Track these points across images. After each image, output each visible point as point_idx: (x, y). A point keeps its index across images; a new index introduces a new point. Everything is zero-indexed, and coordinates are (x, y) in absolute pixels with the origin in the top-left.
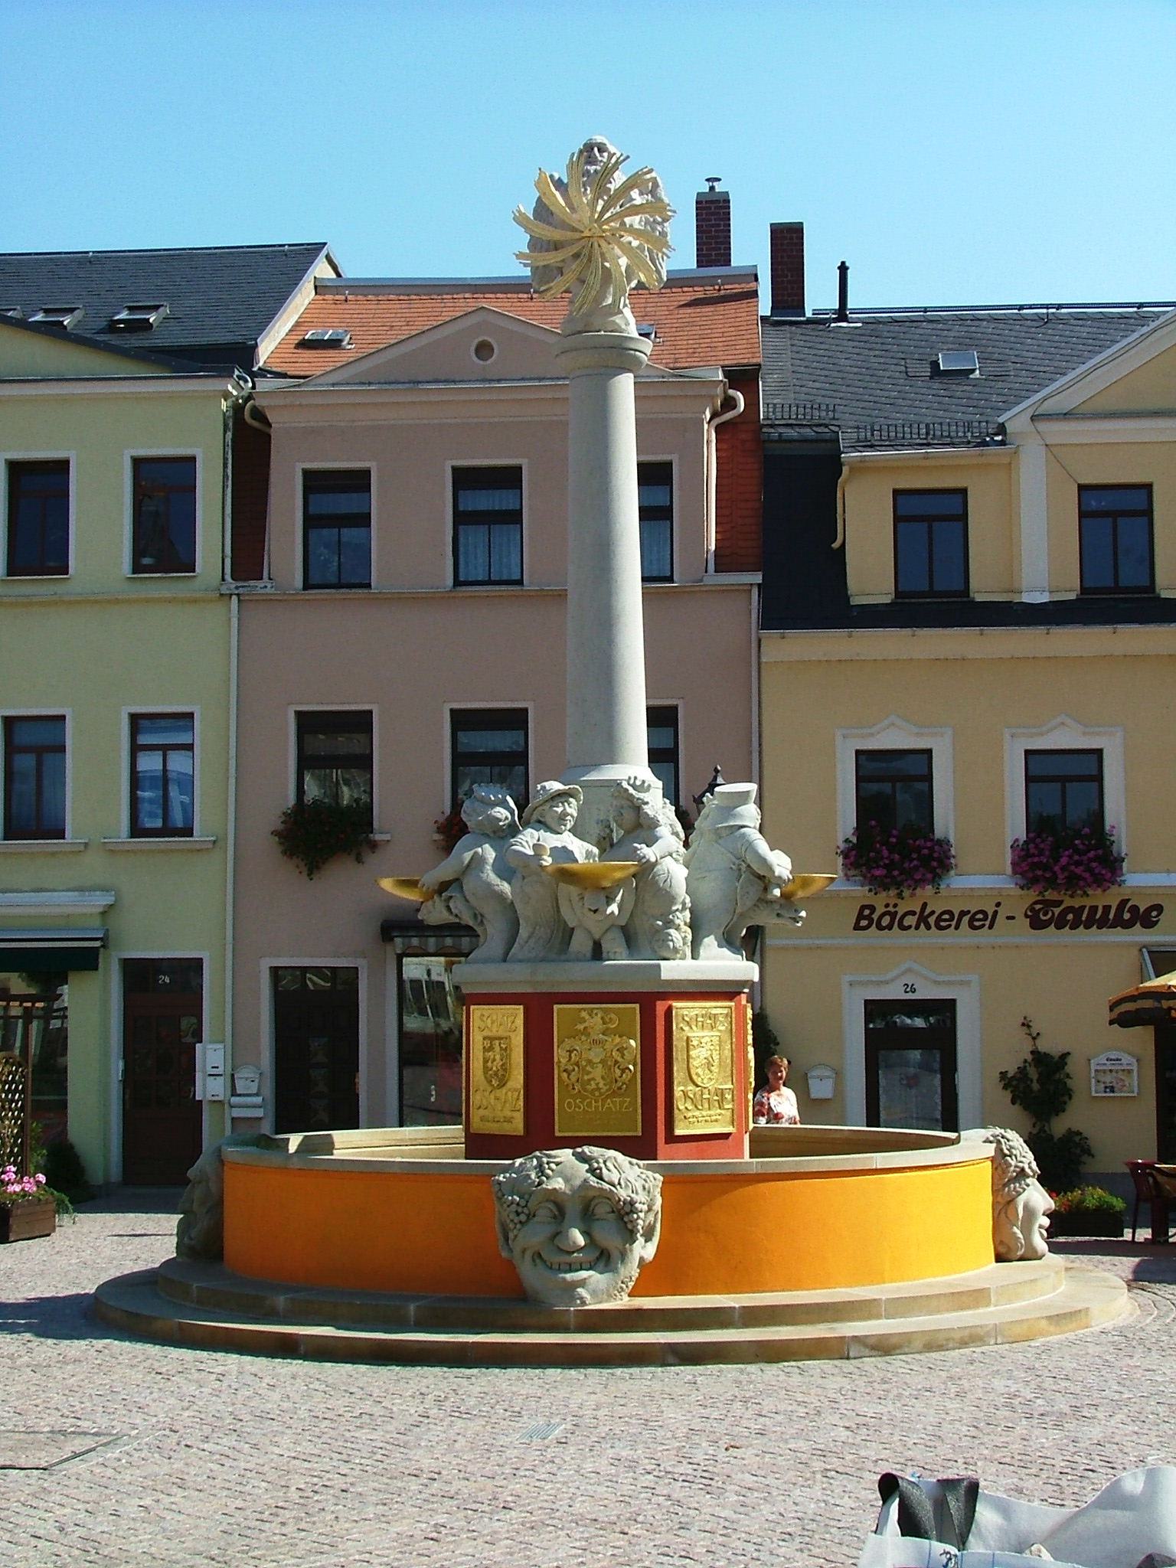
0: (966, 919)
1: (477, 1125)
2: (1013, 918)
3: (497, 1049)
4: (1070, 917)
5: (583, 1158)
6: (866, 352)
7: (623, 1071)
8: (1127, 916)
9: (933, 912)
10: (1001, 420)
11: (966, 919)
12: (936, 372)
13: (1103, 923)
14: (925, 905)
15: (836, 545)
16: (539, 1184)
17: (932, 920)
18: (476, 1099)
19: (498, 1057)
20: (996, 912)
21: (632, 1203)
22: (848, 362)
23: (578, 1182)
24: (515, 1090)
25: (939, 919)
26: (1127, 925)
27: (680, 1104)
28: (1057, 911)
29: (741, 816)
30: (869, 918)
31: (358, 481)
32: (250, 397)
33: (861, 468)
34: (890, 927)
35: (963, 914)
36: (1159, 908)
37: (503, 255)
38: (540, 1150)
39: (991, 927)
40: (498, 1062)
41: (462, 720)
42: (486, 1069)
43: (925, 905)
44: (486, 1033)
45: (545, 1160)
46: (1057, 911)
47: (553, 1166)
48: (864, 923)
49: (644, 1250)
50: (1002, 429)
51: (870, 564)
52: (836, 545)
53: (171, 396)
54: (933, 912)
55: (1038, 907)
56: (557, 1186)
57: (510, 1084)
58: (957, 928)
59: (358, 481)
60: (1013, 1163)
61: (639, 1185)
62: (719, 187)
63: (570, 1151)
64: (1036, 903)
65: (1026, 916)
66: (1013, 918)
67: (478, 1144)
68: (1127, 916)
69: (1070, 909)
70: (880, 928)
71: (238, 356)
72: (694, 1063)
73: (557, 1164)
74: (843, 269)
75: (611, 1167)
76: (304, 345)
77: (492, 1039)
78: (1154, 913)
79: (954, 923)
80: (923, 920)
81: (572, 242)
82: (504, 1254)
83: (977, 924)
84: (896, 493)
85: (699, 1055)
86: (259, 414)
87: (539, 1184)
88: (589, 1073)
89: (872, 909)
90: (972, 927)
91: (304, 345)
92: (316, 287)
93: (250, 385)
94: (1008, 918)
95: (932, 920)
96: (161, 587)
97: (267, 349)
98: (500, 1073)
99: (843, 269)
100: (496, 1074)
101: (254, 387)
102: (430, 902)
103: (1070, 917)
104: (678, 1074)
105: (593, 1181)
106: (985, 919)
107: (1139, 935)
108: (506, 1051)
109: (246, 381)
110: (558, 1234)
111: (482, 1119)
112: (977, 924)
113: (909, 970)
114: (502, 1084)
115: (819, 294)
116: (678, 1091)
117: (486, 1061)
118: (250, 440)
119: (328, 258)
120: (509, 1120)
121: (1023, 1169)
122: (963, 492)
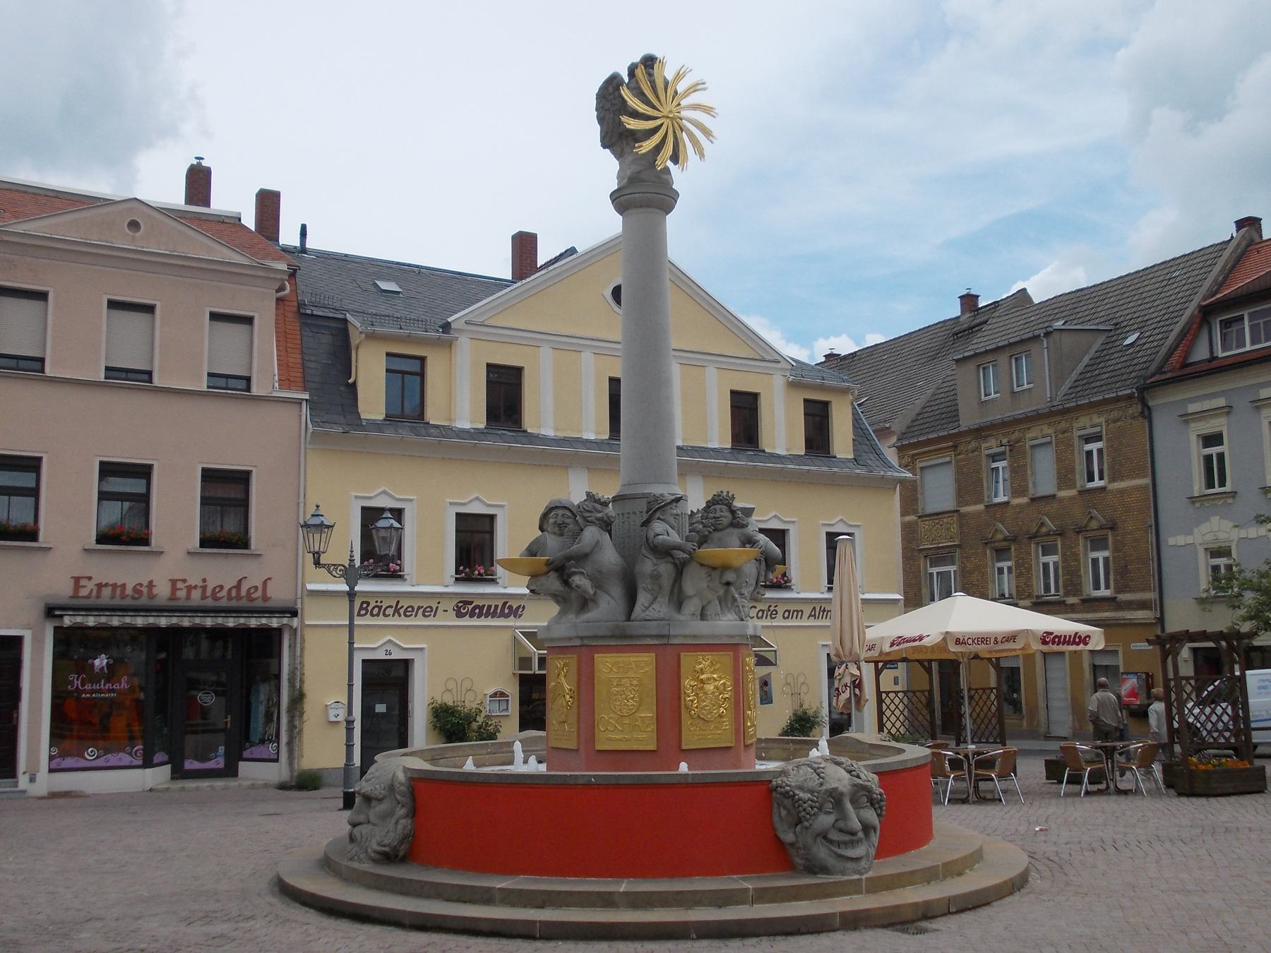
13: (494, 615)
15: (350, 381)
17: (402, 611)
25: (406, 611)
26: (507, 616)
28: (470, 607)
30: (366, 609)
31: (242, 478)
34: (378, 615)
37: (954, 310)
46: (470, 607)
48: (363, 612)
51: (373, 399)
52: (350, 381)
59: (242, 478)
62: (204, 163)
70: (372, 615)
74: (304, 228)
80: (397, 611)
89: (368, 604)
90: (424, 615)
95: (402, 611)
99: (304, 228)
107: (511, 622)
113: (390, 641)
115: (288, 236)
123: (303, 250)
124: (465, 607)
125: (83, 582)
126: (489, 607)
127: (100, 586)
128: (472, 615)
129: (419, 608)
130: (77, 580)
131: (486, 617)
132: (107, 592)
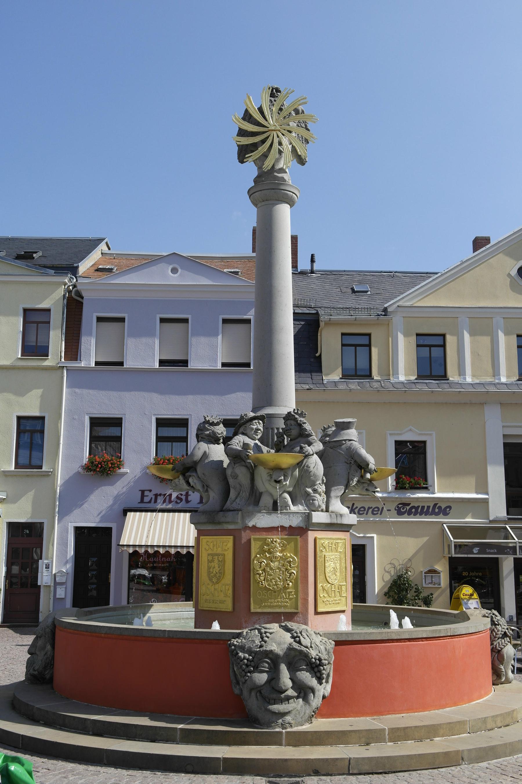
0: (370, 510)
1: (204, 606)
2: (390, 510)
3: (216, 561)
4: (413, 510)
5: (288, 630)
6: (324, 284)
7: (290, 574)
8: (437, 510)
9: (357, 507)
10: (386, 306)
11: (370, 510)
12: (353, 291)
14: (353, 504)
15: (317, 355)
16: (261, 646)
17: (356, 511)
18: (203, 589)
19: (217, 566)
20: (383, 508)
21: (320, 660)
22: (317, 287)
23: (286, 646)
24: (228, 585)
25: (359, 510)
26: (437, 514)
27: (321, 594)
28: (408, 508)
29: (348, 434)
32: (75, 286)
33: (329, 323)
35: (369, 508)
36: (450, 507)
38: (260, 624)
39: (381, 514)
40: (217, 569)
41: (161, 423)
42: (209, 573)
43: (353, 504)
44: (210, 552)
45: (263, 630)
46: (408, 508)
47: (268, 634)
49: (325, 689)
50: (385, 310)
52: (317, 355)
53: (41, 283)
54: (357, 507)
55: (400, 506)
56: (273, 648)
57: (223, 582)
58: (367, 514)
60: (500, 629)
61: (322, 648)
63: (277, 625)
64: (400, 504)
65: (395, 510)
66: (390, 510)
67: (203, 617)
68: (437, 510)
69: (413, 507)
71: (74, 270)
72: (327, 570)
73: (271, 633)
74: (312, 256)
75: (306, 636)
76: (98, 270)
77: (213, 555)
78: (448, 509)
79: (365, 512)
81: (264, 133)
82: (237, 691)
83: (375, 512)
84: (343, 334)
85: (330, 565)
86: (79, 294)
87: (261, 646)
88: (271, 575)
91: (98, 270)
92: (102, 253)
93: (75, 280)
94: (388, 510)
95: (356, 511)
96: (33, 362)
97: (84, 266)
98: (218, 575)
99: (312, 256)
100: (215, 576)
101: (77, 281)
102: (177, 480)
103: (413, 510)
104: (320, 578)
105: (296, 646)
106: (378, 510)
108: (223, 562)
109: (73, 279)
110: (274, 679)
111: (206, 601)
112: (375, 512)
114: (219, 581)
116: (319, 586)
117: (209, 568)
118: (74, 305)
119: (107, 243)
120: (222, 602)
121: (505, 633)
122: (369, 335)
123: (312, 272)
124: (404, 508)
125: (146, 493)
126: (423, 507)
127: (156, 496)
128: (409, 513)
129: (369, 508)
130: (143, 492)
131: (421, 515)
132: (160, 500)
